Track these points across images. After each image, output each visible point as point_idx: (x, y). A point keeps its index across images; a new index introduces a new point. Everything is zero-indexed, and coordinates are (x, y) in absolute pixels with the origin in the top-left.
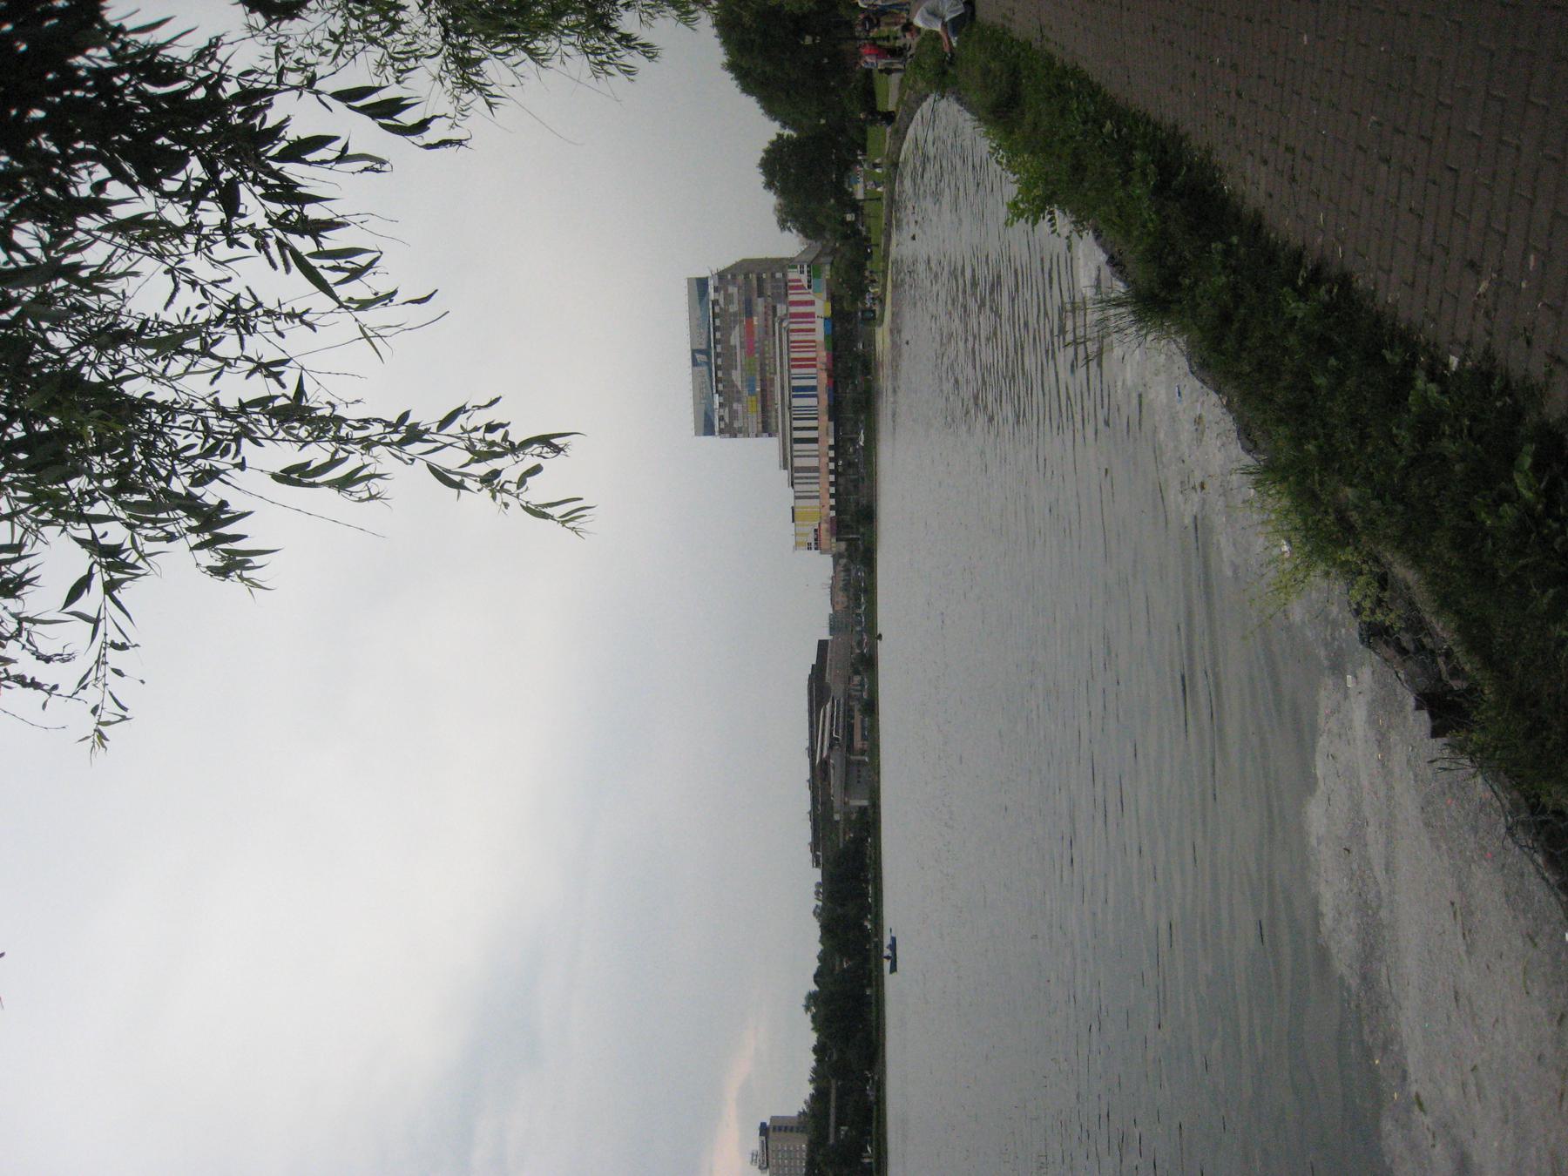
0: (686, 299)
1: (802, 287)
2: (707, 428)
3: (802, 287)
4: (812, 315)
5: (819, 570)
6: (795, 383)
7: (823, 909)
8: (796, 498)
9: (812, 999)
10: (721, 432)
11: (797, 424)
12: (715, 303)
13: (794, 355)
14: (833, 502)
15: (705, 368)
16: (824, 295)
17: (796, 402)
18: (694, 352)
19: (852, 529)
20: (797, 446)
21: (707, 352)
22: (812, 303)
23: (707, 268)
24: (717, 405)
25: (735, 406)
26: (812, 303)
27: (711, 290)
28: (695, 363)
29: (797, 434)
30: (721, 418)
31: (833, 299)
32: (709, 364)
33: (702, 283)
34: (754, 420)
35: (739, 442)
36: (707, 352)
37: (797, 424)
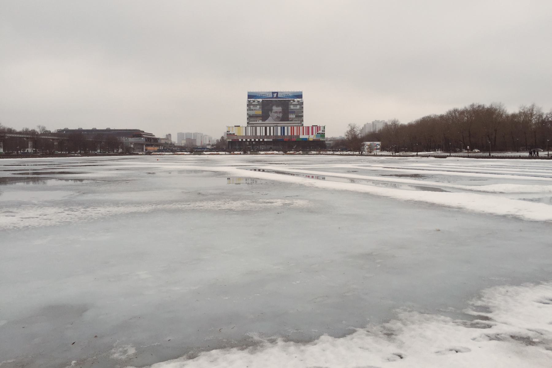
0: (295, 91)
1: (318, 131)
2: (250, 96)
3: (318, 131)
4: (308, 134)
5: (216, 134)
6: (286, 128)
7: (375, 134)
8: (308, 127)
9: (386, 125)
10: (249, 101)
11: (272, 128)
12: (294, 101)
13: (295, 127)
14: (244, 140)
15: (271, 96)
16: (315, 138)
17: (279, 128)
18: (277, 93)
19: (231, 145)
20: (264, 128)
21: (277, 97)
22: (312, 134)
23: (305, 99)
24: (258, 100)
25: (258, 106)
26: (312, 134)
27: (299, 100)
28: (273, 93)
29: (268, 128)
30: (254, 101)
31: (314, 141)
32: (273, 98)
33: (300, 96)
34: (252, 113)
35: (246, 108)
36: (277, 97)
37: (272, 128)
